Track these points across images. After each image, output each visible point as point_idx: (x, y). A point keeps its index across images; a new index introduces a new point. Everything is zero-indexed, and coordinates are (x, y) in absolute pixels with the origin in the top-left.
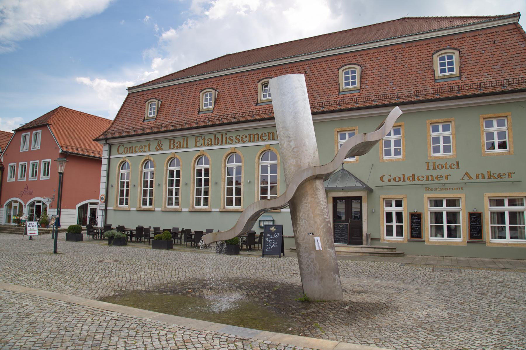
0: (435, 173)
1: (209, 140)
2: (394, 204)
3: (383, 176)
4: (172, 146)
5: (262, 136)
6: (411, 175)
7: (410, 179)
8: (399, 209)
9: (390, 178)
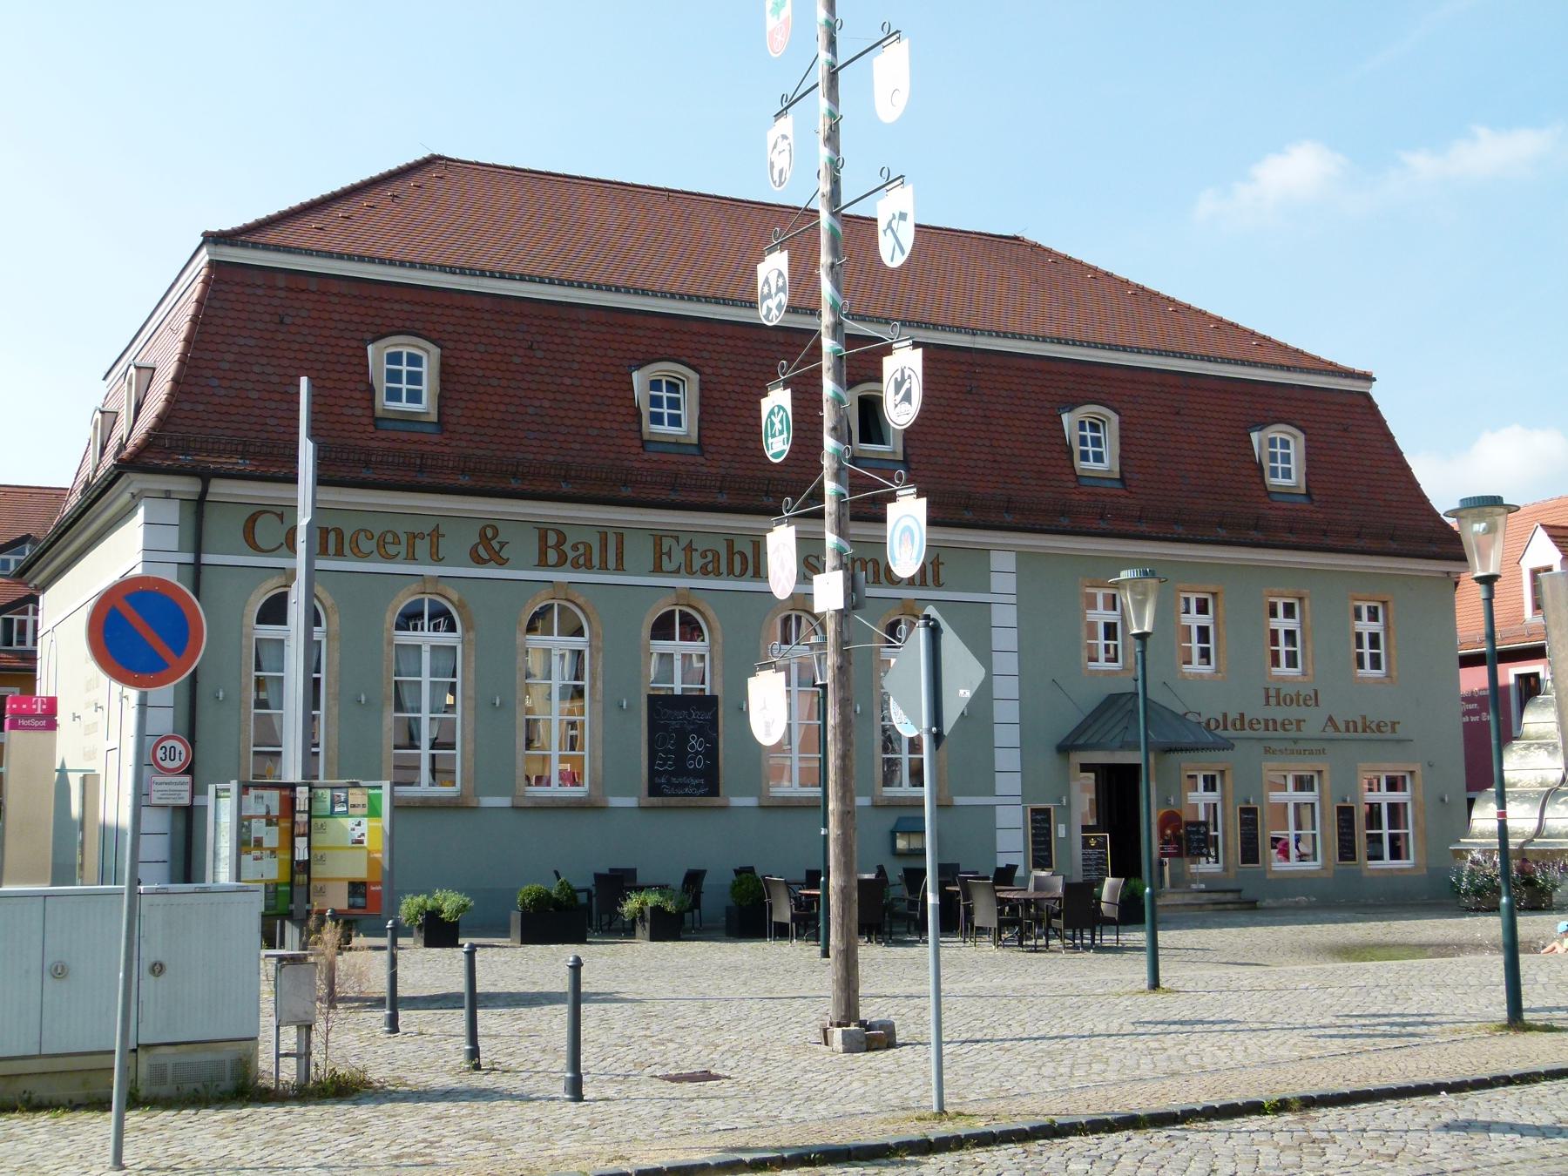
0: (1279, 713)
1: (710, 555)
4: (552, 556)
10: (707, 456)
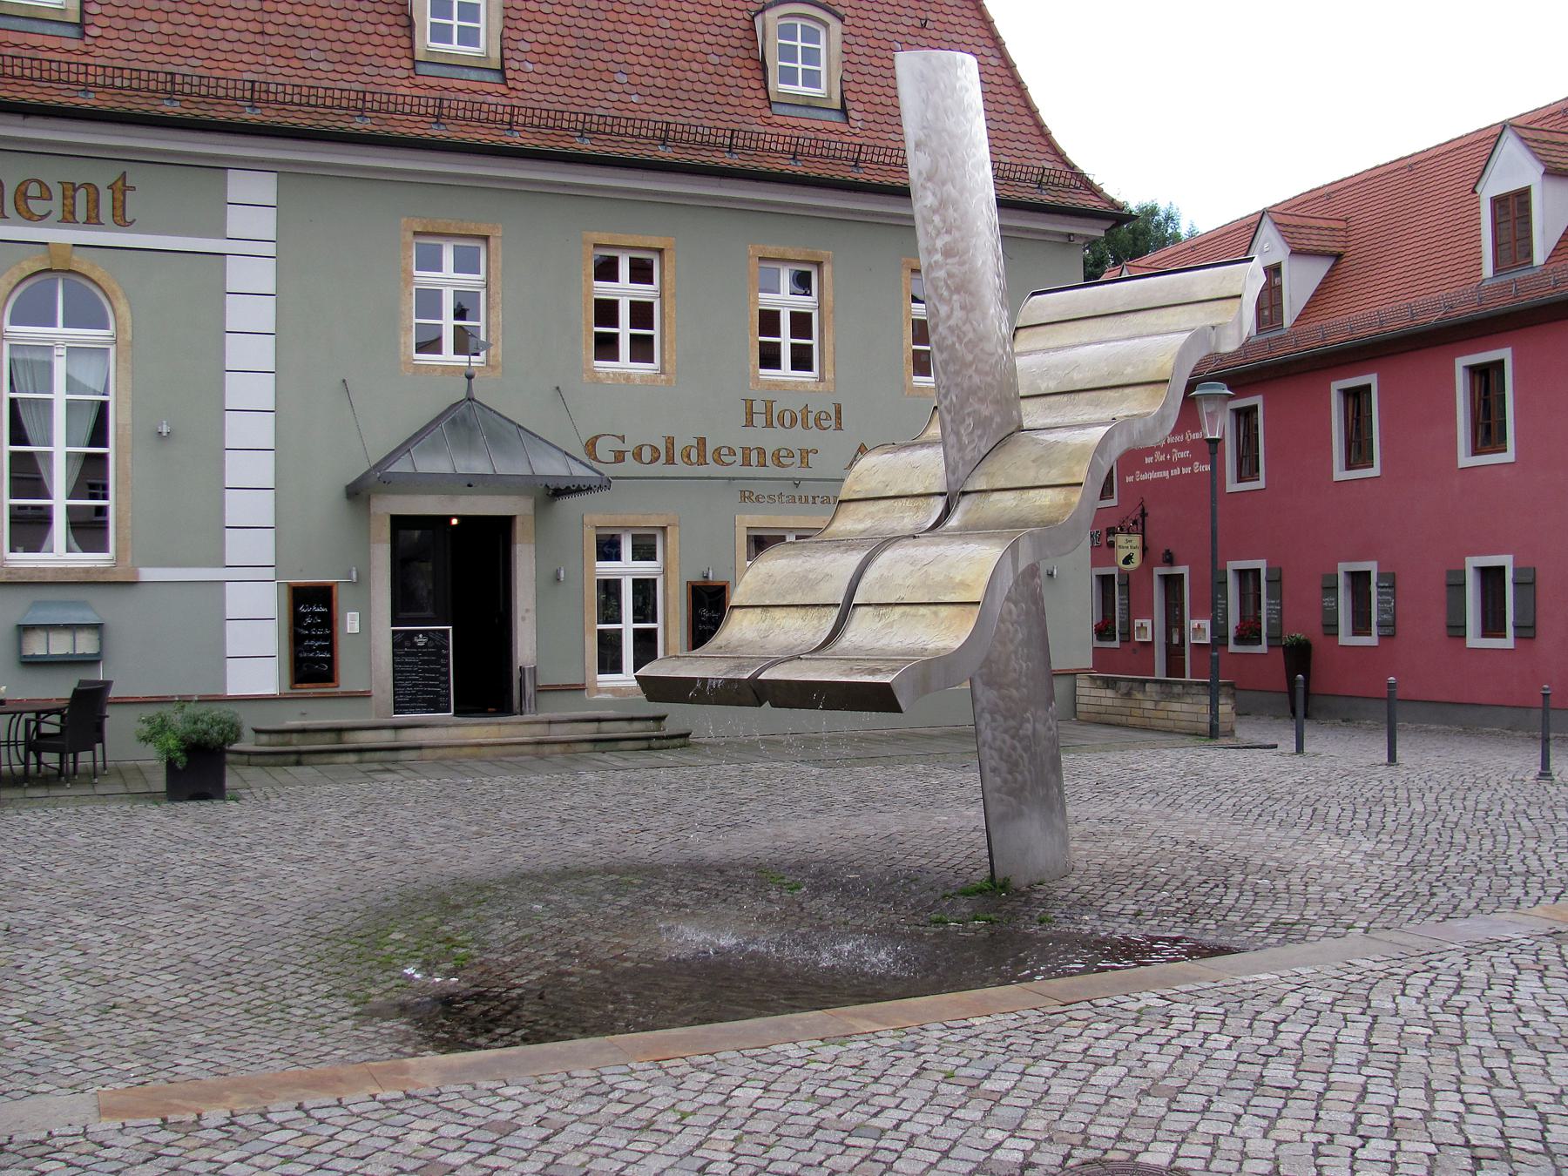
0: (772, 439)
2: (626, 548)
3: (597, 438)
5: (22, 195)
8: (646, 568)
10: (510, 84)
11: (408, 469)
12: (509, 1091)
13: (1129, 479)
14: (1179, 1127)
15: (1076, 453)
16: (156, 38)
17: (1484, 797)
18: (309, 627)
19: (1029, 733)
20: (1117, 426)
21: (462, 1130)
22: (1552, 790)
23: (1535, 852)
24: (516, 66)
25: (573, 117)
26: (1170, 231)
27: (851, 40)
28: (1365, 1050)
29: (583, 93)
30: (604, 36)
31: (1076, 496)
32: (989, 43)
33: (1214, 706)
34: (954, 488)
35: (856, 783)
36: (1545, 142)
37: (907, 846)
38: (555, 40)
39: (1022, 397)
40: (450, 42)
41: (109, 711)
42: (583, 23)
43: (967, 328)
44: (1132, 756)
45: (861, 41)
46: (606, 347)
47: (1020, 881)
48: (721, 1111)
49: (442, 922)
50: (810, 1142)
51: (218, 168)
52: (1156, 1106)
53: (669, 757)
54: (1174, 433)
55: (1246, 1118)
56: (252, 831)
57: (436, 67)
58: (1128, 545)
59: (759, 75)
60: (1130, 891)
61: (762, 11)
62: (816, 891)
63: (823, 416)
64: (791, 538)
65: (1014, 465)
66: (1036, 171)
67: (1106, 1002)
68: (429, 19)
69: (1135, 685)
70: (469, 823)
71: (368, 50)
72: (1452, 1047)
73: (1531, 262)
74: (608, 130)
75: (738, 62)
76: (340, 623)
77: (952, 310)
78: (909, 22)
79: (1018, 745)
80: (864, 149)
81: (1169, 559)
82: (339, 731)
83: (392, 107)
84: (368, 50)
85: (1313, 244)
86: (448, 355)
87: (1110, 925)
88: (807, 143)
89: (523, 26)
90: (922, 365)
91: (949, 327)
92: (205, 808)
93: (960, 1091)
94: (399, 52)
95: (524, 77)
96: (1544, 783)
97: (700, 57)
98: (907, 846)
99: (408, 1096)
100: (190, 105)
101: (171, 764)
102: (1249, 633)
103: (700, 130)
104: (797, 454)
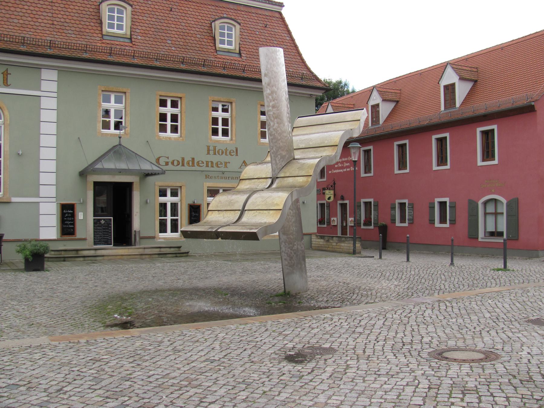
0: (215, 159)
3: (160, 157)
6: (191, 159)
7: (189, 164)
8: (175, 199)
9: (167, 160)
11: (101, 167)
12: (159, 335)
13: (330, 172)
14: (332, 340)
15: (310, 166)
16: (17, 25)
17: (433, 270)
18: (67, 217)
19: (296, 248)
20: (322, 158)
21: (149, 343)
22: (453, 268)
23: (443, 284)
24: (135, 37)
25: (154, 54)
26: (346, 89)
27: (242, 31)
28: (382, 325)
29: (157, 46)
30: (164, 28)
31: (310, 179)
32: (287, 32)
33: (354, 245)
34: (274, 176)
35: (243, 267)
36: (460, 69)
37: (259, 283)
38: (148, 29)
39: (295, 149)
40: (114, 28)
41: (3, 244)
42: (157, 24)
43: (278, 129)
44: (328, 259)
45: (246, 31)
46: (163, 129)
47: (293, 292)
48: (216, 338)
49: (123, 303)
50: (239, 343)
51: (39, 68)
52: (327, 336)
53: (183, 259)
54: (341, 158)
55: (349, 338)
56: (57, 279)
57: (110, 37)
58: (329, 194)
59: (213, 42)
60: (325, 295)
61: (214, 21)
62: (233, 295)
63: (232, 151)
64: (221, 191)
65: (292, 170)
66: (301, 74)
67: (316, 316)
68: (107, 21)
69: (330, 238)
70: (124, 277)
71: (87, 31)
72: (405, 324)
73: (455, 106)
74: (165, 59)
75: (206, 37)
76: (77, 216)
77: (274, 124)
78: (261, 25)
79: (292, 252)
80: (246, 66)
81: (343, 198)
82: (77, 250)
83: (95, 50)
84: (87, 31)
85: (390, 97)
86: (112, 130)
87: (319, 304)
88: (228, 64)
89: (137, 24)
90: (263, 135)
91: (273, 129)
92: (39, 273)
93: (277, 334)
94: (97, 32)
95: (138, 41)
96: (452, 266)
97: (194, 35)
98: (259, 283)
99: (132, 337)
100: (30, 47)
101: (26, 260)
102: (368, 222)
103: (194, 59)
104: (223, 163)
